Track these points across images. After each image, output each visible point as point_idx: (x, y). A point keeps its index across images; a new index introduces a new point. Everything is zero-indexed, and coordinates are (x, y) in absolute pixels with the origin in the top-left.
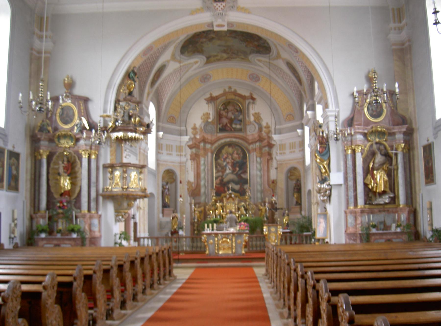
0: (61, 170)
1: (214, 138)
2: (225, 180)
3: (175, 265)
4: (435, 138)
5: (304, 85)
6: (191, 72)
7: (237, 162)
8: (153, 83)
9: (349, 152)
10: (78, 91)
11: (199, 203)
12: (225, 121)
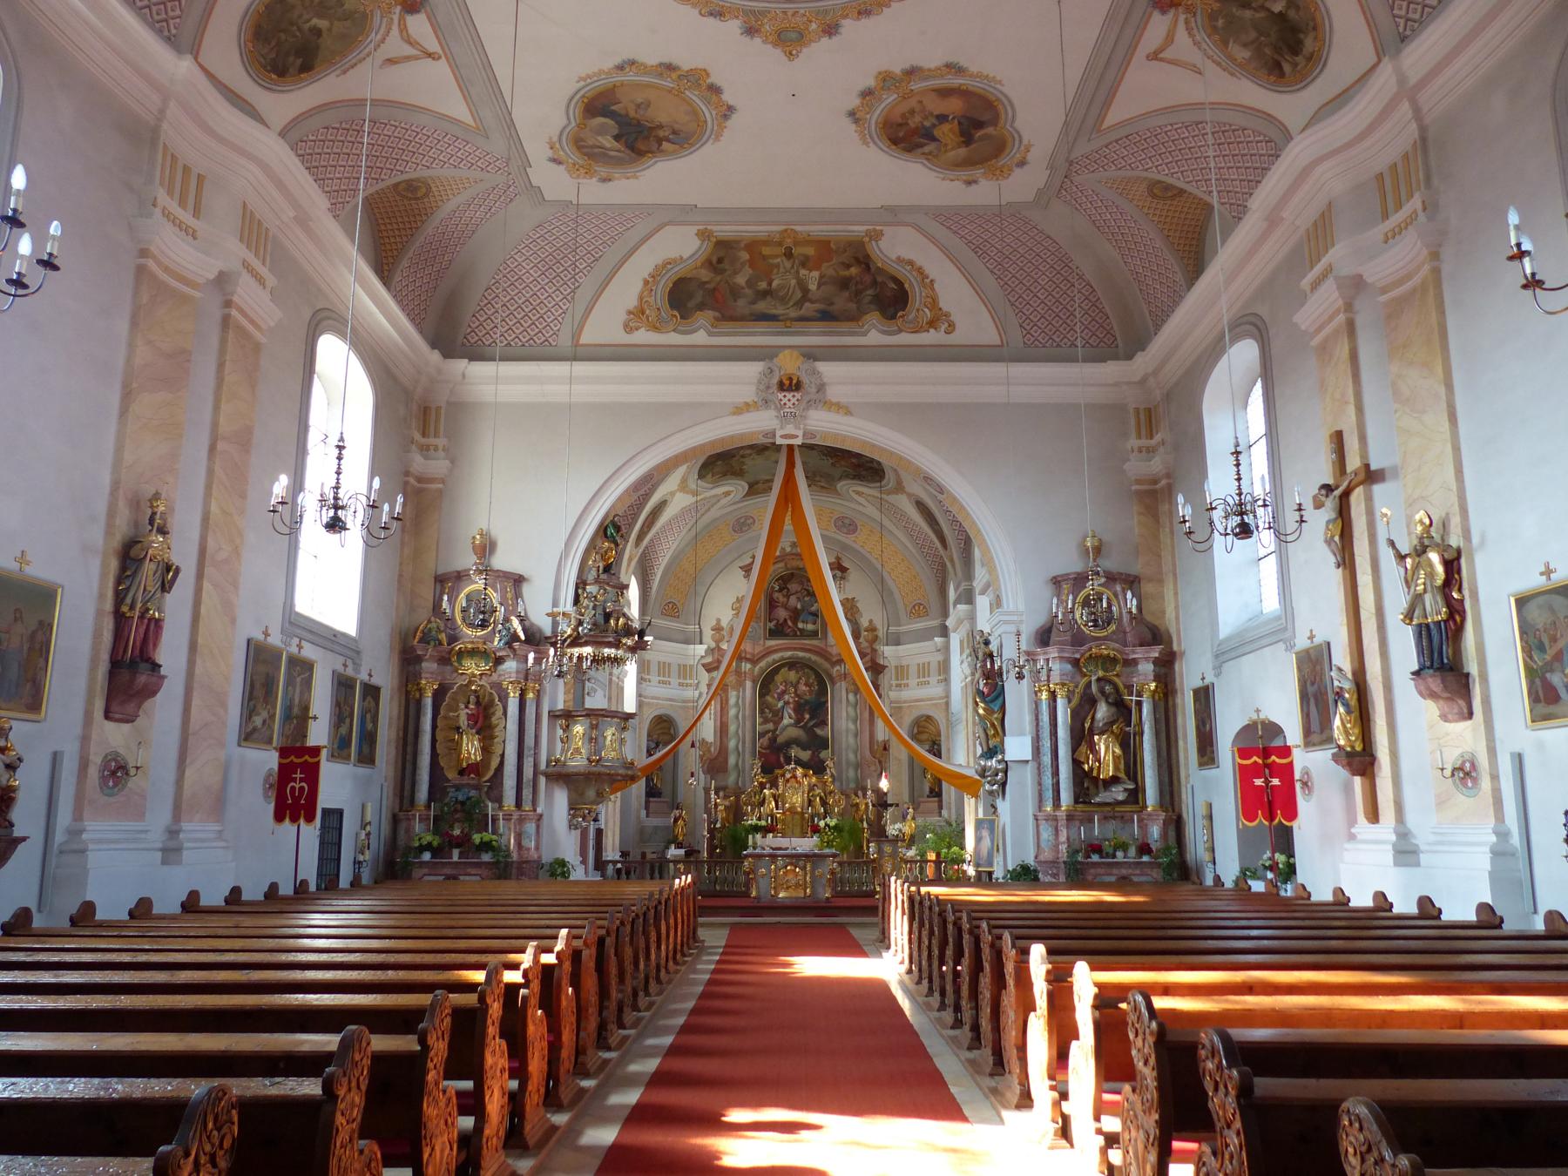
0: (463, 721)
1: (758, 649)
2: (780, 740)
3: (700, 920)
4: (1217, 675)
5: (948, 551)
6: (715, 513)
7: (807, 702)
8: (640, 538)
9: (1044, 696)
10: (500, 562)
11: (724, 788)
12: (782, 614)
